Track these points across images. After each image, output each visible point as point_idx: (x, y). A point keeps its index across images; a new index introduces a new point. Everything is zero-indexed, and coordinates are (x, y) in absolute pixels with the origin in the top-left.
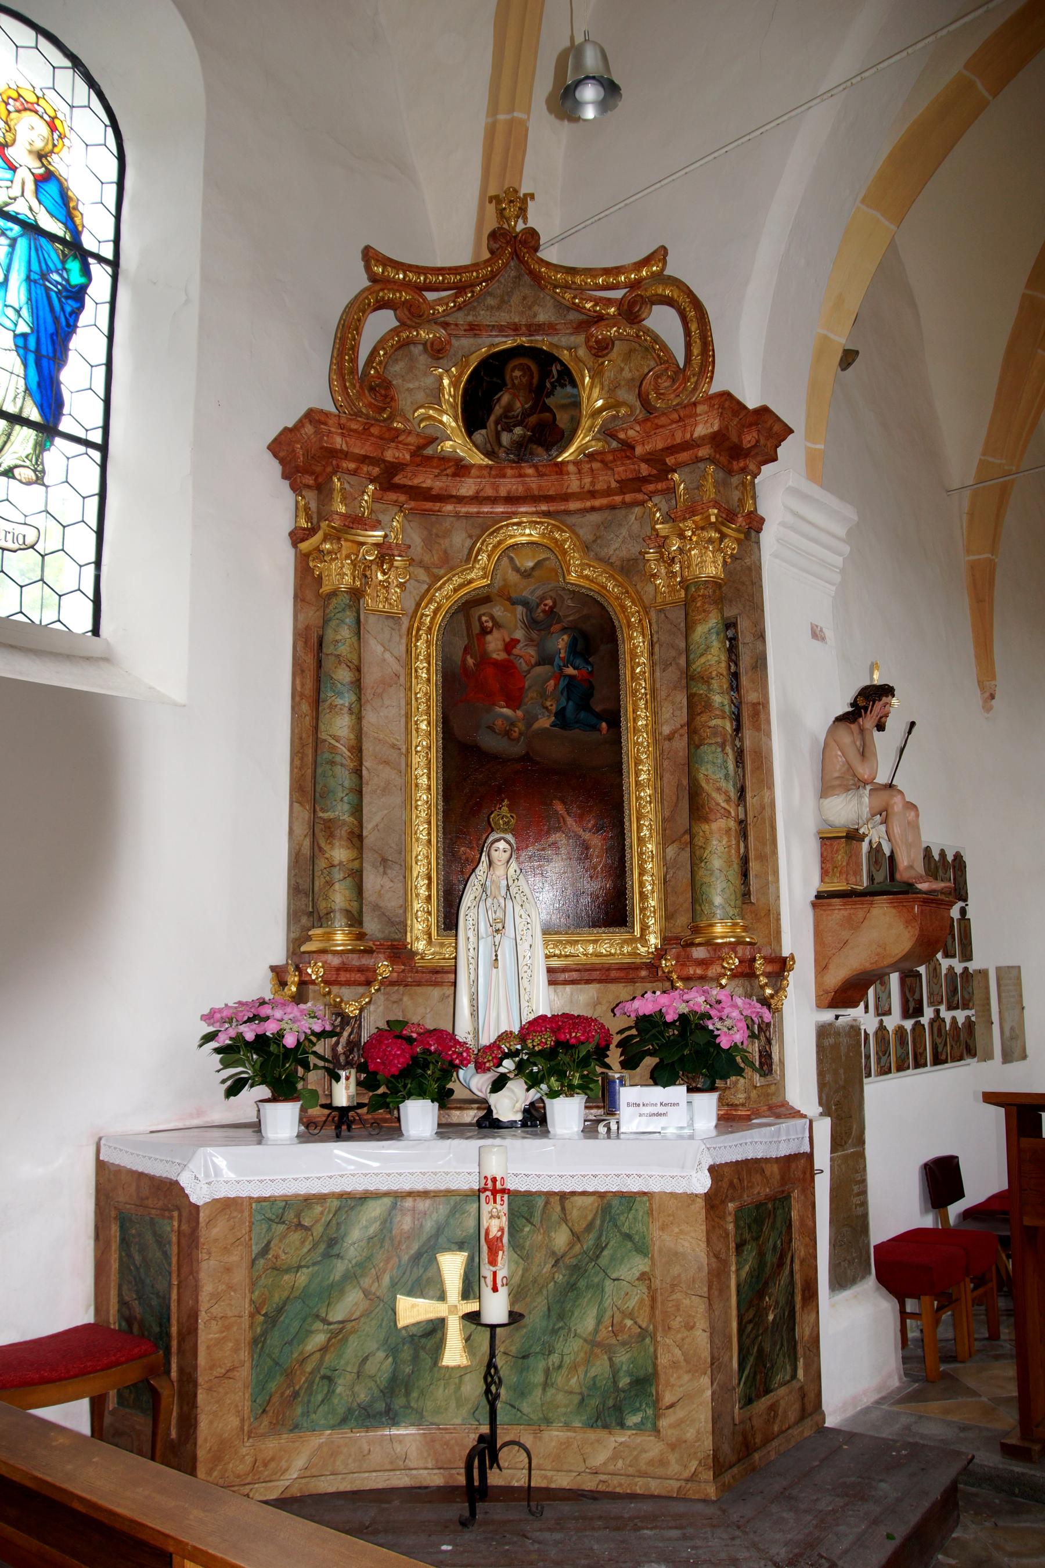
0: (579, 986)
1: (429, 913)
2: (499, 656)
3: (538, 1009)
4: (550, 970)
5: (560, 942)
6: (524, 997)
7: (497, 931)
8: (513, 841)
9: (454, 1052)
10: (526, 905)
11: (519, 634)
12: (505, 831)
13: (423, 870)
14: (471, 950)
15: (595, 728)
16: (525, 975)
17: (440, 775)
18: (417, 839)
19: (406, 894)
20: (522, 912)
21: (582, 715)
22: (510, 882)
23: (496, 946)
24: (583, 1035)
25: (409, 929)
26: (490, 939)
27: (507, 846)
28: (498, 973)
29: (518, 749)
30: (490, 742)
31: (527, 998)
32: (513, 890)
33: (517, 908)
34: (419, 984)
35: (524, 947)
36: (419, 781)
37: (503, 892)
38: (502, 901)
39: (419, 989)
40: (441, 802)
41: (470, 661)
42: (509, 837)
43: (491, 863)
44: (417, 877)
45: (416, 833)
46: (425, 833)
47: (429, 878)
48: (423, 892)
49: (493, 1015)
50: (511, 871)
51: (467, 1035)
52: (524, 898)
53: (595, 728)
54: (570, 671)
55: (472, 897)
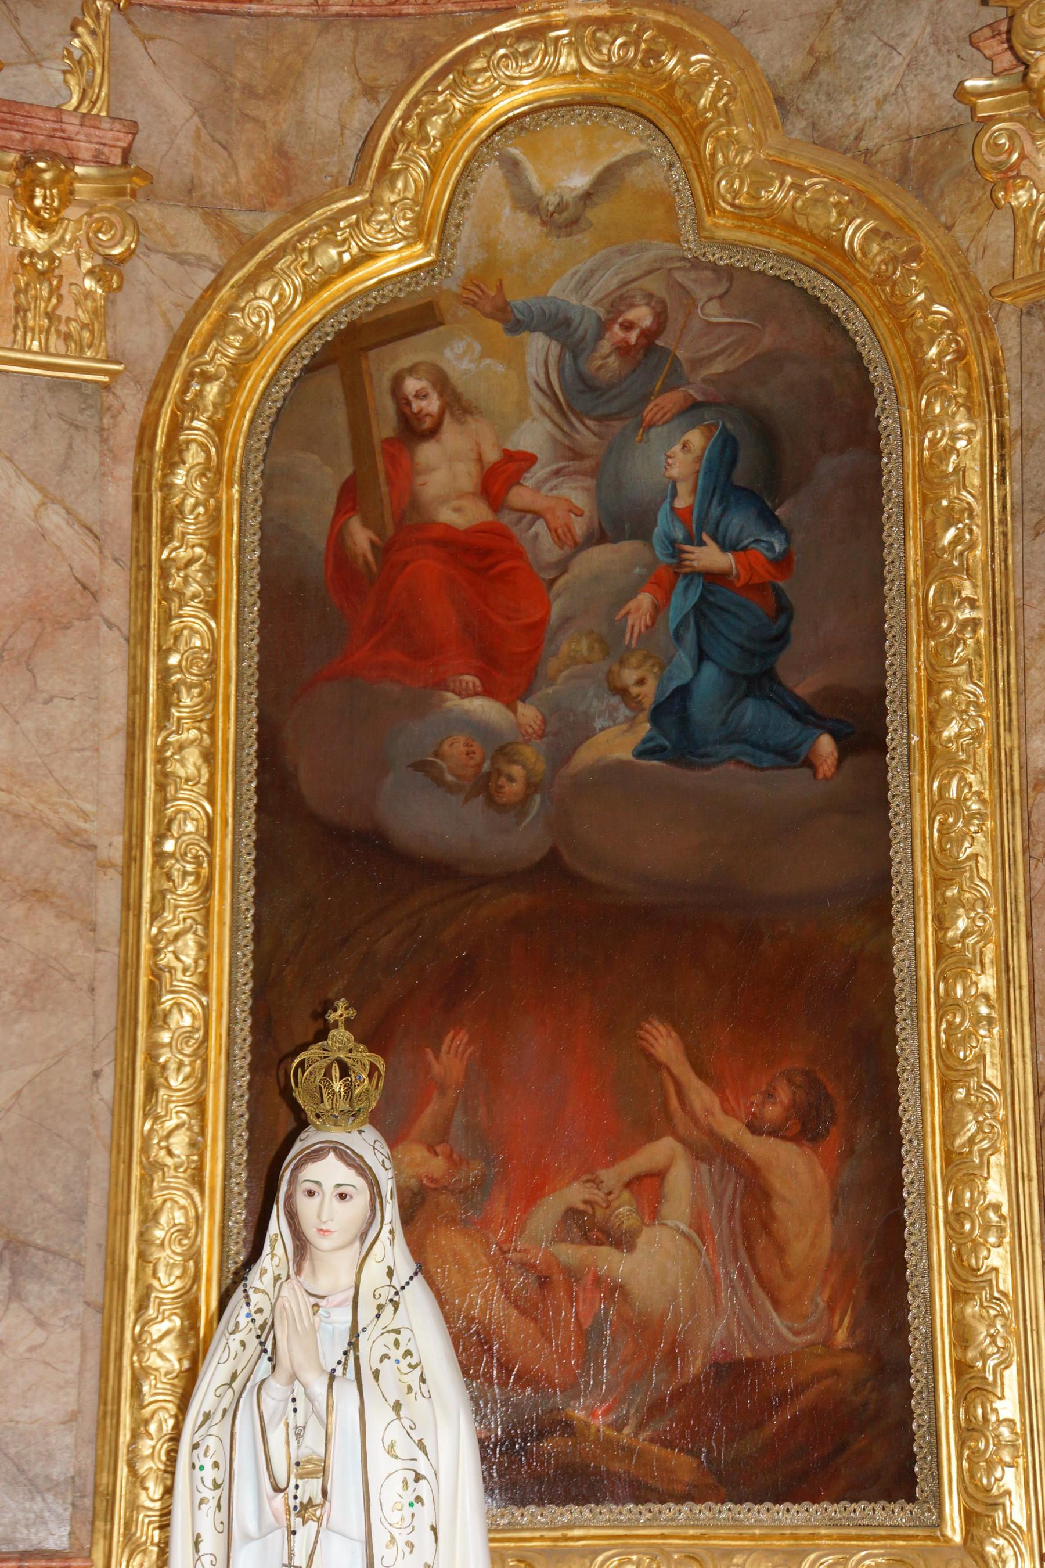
2: (463, 516)
7: (304, 1509)
10: (416, 1407)
11: (533, 436)
13: (168, 1282)
15: (793, 757)
20: (396, 1433)
21: (750, 711)
27: (347, 1175)
29: (524, 841)
30: (428, 820)
32: (370, 1348)
33: (379, 1415)
36: (167, 958)
37: (332, 1352)
38: (319, 1388)
41: (361, 537)
42: (367, 1143)
43: (301, 1245)
50: (374, 1274)
52: (413, 1378)
53: (793, 757)
54: (710, 557)
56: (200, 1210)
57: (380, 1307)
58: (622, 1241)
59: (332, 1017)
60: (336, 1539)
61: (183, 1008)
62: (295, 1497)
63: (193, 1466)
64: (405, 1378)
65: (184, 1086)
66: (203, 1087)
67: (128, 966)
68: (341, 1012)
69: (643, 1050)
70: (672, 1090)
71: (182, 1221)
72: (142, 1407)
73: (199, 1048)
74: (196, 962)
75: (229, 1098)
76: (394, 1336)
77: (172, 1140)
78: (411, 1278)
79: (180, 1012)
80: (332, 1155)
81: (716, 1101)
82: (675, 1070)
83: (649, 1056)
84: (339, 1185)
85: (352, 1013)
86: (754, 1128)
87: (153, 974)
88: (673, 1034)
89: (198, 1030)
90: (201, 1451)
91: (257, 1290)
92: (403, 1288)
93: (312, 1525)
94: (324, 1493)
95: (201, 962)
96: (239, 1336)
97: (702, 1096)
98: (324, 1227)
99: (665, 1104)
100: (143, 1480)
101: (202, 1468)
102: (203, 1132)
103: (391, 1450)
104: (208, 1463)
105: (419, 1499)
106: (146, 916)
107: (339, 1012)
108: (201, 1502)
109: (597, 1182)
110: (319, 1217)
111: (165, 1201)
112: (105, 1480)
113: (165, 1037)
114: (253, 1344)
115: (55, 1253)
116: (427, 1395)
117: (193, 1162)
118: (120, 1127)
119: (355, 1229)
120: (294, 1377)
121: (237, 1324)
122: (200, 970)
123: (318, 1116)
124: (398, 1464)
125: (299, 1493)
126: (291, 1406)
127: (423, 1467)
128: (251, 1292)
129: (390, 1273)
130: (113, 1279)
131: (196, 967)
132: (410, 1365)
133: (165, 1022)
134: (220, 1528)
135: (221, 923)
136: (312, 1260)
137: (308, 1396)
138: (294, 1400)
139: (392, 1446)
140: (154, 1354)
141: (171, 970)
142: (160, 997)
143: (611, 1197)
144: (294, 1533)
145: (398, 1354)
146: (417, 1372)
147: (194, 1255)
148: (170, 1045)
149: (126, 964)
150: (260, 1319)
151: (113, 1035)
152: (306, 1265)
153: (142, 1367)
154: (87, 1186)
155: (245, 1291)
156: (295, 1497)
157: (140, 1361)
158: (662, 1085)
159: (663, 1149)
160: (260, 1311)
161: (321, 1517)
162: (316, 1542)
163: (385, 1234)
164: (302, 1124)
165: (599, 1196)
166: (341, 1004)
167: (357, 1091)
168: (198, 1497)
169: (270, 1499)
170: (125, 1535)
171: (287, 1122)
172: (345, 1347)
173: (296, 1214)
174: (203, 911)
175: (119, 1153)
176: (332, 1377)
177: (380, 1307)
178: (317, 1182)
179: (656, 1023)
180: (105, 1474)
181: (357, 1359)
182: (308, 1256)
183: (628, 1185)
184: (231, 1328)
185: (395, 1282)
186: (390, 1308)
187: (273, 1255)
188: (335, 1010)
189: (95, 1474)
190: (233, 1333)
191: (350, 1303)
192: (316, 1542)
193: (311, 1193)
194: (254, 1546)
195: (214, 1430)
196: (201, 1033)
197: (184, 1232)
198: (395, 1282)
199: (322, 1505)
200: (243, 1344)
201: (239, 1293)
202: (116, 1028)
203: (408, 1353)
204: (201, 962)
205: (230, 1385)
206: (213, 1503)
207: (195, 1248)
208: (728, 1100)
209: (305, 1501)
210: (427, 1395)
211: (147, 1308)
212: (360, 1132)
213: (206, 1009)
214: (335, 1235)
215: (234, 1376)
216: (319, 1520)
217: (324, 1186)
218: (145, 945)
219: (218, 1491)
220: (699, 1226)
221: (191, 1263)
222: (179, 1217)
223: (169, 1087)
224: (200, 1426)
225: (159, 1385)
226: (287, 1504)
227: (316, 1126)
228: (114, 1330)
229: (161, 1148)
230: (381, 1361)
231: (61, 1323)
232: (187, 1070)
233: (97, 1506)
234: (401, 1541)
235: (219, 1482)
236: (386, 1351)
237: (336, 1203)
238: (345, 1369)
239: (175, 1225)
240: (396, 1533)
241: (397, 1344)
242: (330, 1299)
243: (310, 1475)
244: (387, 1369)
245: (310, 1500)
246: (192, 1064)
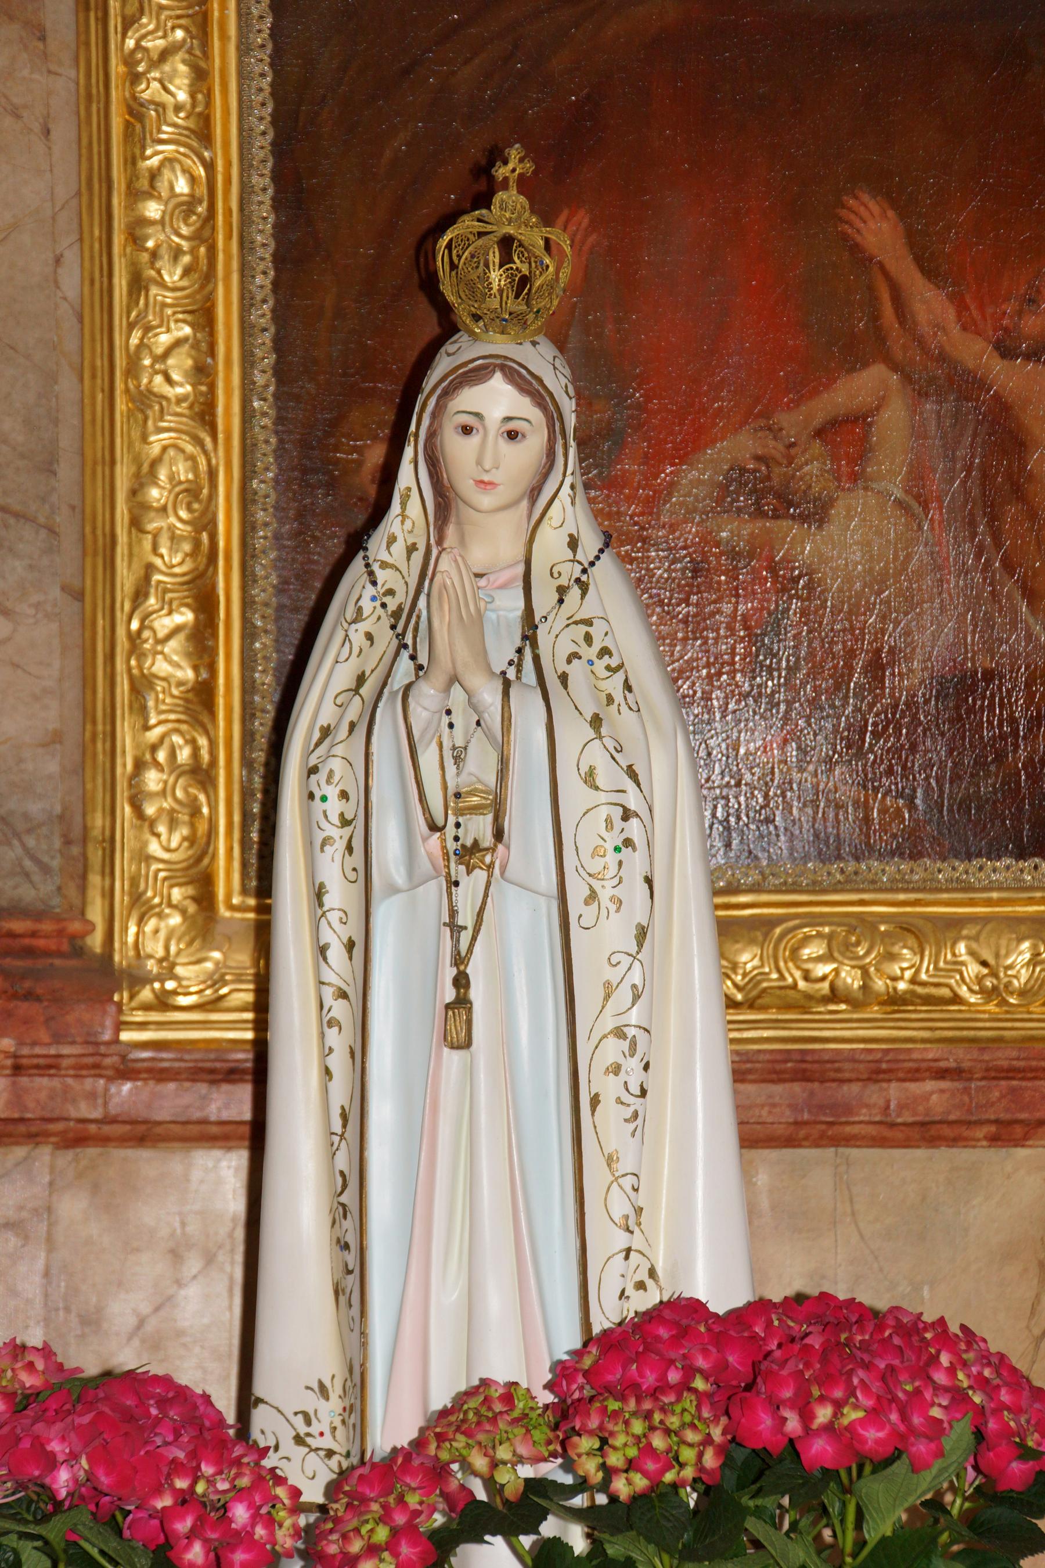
0: (963, 1155)
1: (201, 774)
3: (682, 1263)
4: (745, 1069)
5: (865, 925)
6: (607, 1204)
7: (469, 854)
8: (557, 381)
9: (185, 1500)
10: (623, 722)
12: (513, 323)
13: (173, 562)
14: (336, 953)
16: (610, 1088)
17: (261, 63)
18: (144, 401)
19: (88, 682)
20: (597, 756)
22: (544, 599)
23: (460, 936)
24: (874, 1416)
25: (95, 856)
26: (433, 890)
27: (524, 407)
28: (470, 1073)
31: (620, 1207)
32: (556, 642)
33: (573, 734)
34: (144, 1133)
35: (604, 938)
36: (150, 91)
37: (502, 651)
38: (490, 696)
39: (147, 1162)
40: (264, 209)
42: (541, 359)
43: (445, 503)
44: (140, 595)
45: (133, 369)
46: (180, 364)
47: (205, 603)
48: (172, 667)
49: (447, 1295)
50: (551, 544)
51: (311, 1402)
52: (614, 685)
55: (344, 677)
56: (214, 461)
57: (562, 591)
58: (817, 514)
59: (501, 172)
60: (511, 891)
61: (178, 167)
62: (456, 839)
63: (311, 796)
64: (603, 685)
65: (185, 283)
66: (210, 287)
67: (93, 97)
68: (514, 165)
69: (845, 237)
70: (885, 296)
71: (190, 476)
72: (147, 728)
73: (202, 227)
74: (193, 96)
75: (247, 303)
76: (583, 629)
77: (171, 361)
78: (601, 551)
79: (173, 170)
80: (498, 375)
81: (951, 314)
82: (892, 267)
83: (855, 249)
84: (509, 419)
85: (529, 166)
86: (1006, 351)
87: (131, 112)
88: (890, 213)
89: (200, 202)
90: (322, 776)
91: (384, 565)
92: (592, 564)
93: (480, 875)
94: (499, 835)
95: (200, 96)
96: (363, 627)
97: (930, 304)
98: (486, 478)
99: (875, 317)
100: (152, 823)
101: (324, 799)
102: (212, 352)
103: (590, 779)
104: (332, 792)
105: (628, 843)
106: (114, 22)
107: (511, 166)
108: (326, 842)
109: (775, 432)
110: (479, 462)
111: (165, 449)
112: (99, 822)
113: (153, 210)
114: (385, 638)
115: (17, 515)
116: (635, 708)
117: (202, 393)
118: (93, 340)
119: (525, 482)
120: (454, 679)
121: (360, 610)
122: (198, 109)
123: (477, 318)
124: (603, 797)
125: (461, 832)
126: (446, 720)
127: (633, 800)
128: (376, 567)
129: (573, 543)
130: (95, 554)
131: (194, 105)
132: (608, 668)
133: (152, 186)
134: (352, 876)
135: (224, 37)
136: (459, 523)
137: (472, 703)
138: (449, 712)
139: (591, 772)
140: (159, 657)
141: (160, 106)
142: (143, 148)
143: (793, 451)
144: (456, 884)
145: (592, 652)
146: (620, 677)
147: (205, 523)
148: (162, 222)
149: (89, 97)
150: (392, 604)
151: (74, 202)
152: (451, 530)
153: (143, 675)
154: (56, 422)
155: (367, 565)
156: (456, 839)
157: (140, 667)
158: (871, 288)
159: (865, 385)
160: (391, 592)
161: (492, 863)
162: (486, 895)
163: (566, 489)
164: (449, 329)
165: (774, 448)
166: (514, 153)
167: (538, 283)
168: (319, 836)
169: (425, 840)
170: (131, 894)
171: (432, 328)
172: (518, 643)
173: (438, 461)
174: (199, 18)
175: (93, 377)
176: (507, 684)
177: (562, 591)
178: (478, 415)
179: (866, 198)
180: (99, 815)
181: (536, 659)
182: (453, 519)
183: (819, 433)
184: (350, 614)
185: (580, 556)
186: (575, 592)
187: (404, 516)
188: (506, 163)
189: (84, 815)
190: (354, 621)
191: (521, 584)
192: (486, 895)
193: (467, 430)
194: (397, 900)
195: (339, 750)
196: (205, 204)
197: (192, 492)
198: (580, 556)
199: (493, 850)
200: (369, 637)
201: (357, 565)
202: (79, 193)
203: (605, 652)
204: (200, 96)
205: (356, 691)
206: (340, 845)
207: (209, 516)
208: (967, 309)
209: (469, 843)
210: (635, 708)
211: (146, 595)
212: (534, 344)
213: (209, 167)
214: (501, 488)
215: (361, 679)
216: (490, 867)
217: (488, 422)
218: (117, 68)
219: (348, 830)
220: (918, 498)
221: (205, 536)
222: (184, 473)
223: (163, 285)
224: (317, 745)
225: (168, 700)
226: (444, 848)
227: (471, 333)
228: (100, 622)
229: (157, 372)
230: (569, 662)
231: (32, 611)
232: (186, 259)
233: (90, 855)
234: (605, 894)
235: (349, 816)
236: (574, 648)
237: (505, 447)
238: (519, 671)
239: (180, 483)
240: (597, 885)
241: (588, 639)
242: (492, 577)
243: (476, 809)
244: (576, 671)
245: (476, 842)
246: (193, 251)
